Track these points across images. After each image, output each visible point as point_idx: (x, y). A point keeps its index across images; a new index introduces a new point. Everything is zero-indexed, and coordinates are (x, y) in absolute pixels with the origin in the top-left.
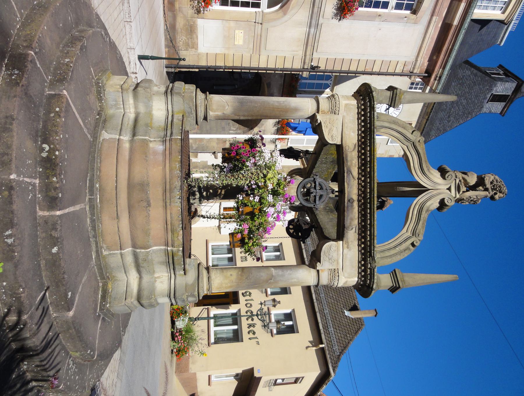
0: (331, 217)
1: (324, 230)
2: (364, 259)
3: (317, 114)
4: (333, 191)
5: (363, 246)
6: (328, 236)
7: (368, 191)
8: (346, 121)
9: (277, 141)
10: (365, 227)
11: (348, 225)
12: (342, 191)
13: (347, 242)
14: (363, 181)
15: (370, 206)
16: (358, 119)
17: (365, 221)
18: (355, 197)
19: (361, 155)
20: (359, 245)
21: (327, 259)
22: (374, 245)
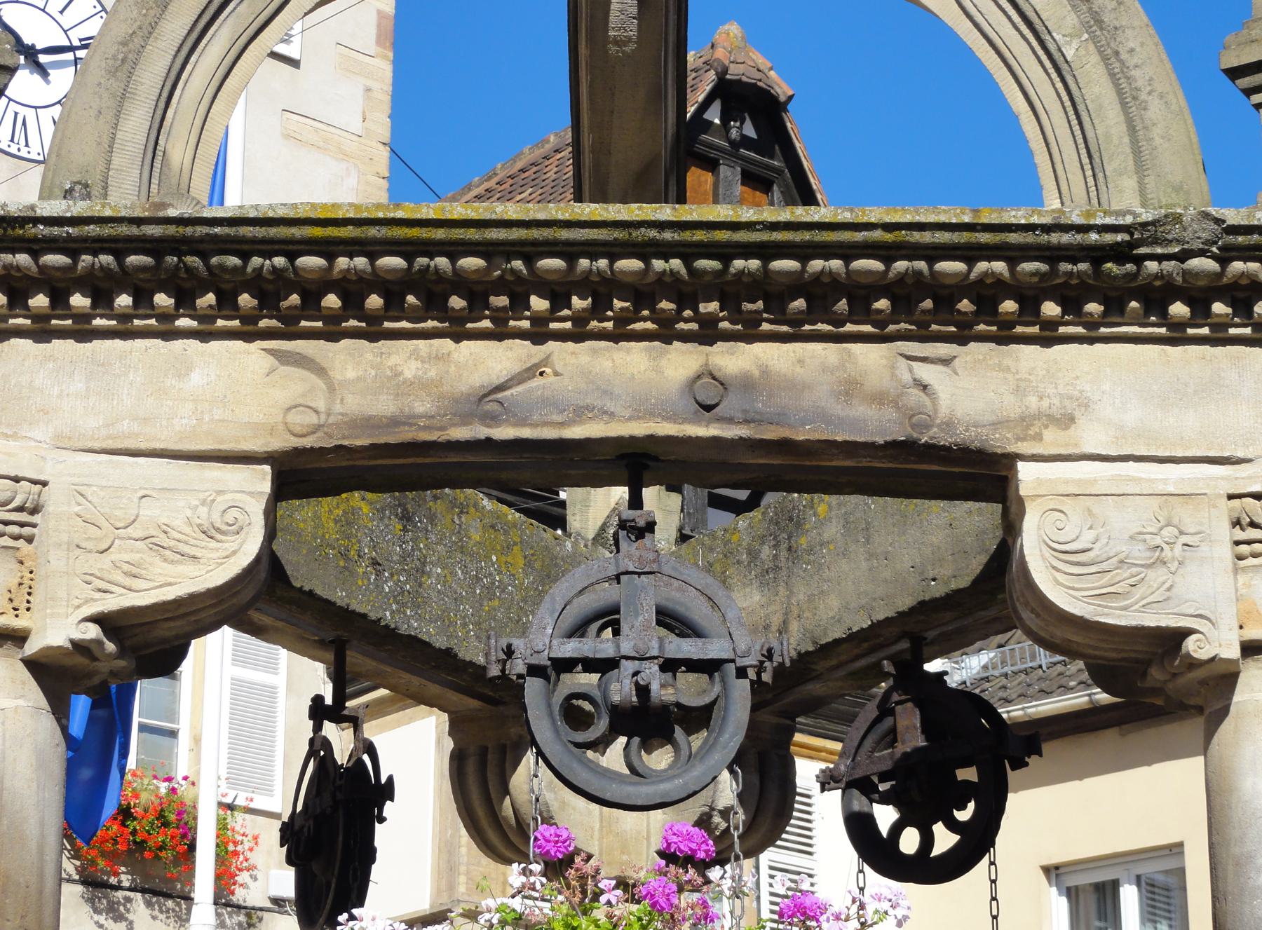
0: (833, 530)
1: (937, 590)
2: (1156, 298)
3: (31, 648)
4: (636, 529)
5: (1051, 309)
6: (976, 564)
7: (633, 264)
8: (92, 425)
9: (239, 895)
10: (905, 294)
11: (890, 414)
12: (634, 463)
13: (1027, 423)
14: (559, 299)
15: (747, 251)
16: (83, 333)
17: (860, 294)
18: (680, 362)
19: (362, 315)
20: (1049, 337)
21: (1157, 576)
22: (1047, 229)
